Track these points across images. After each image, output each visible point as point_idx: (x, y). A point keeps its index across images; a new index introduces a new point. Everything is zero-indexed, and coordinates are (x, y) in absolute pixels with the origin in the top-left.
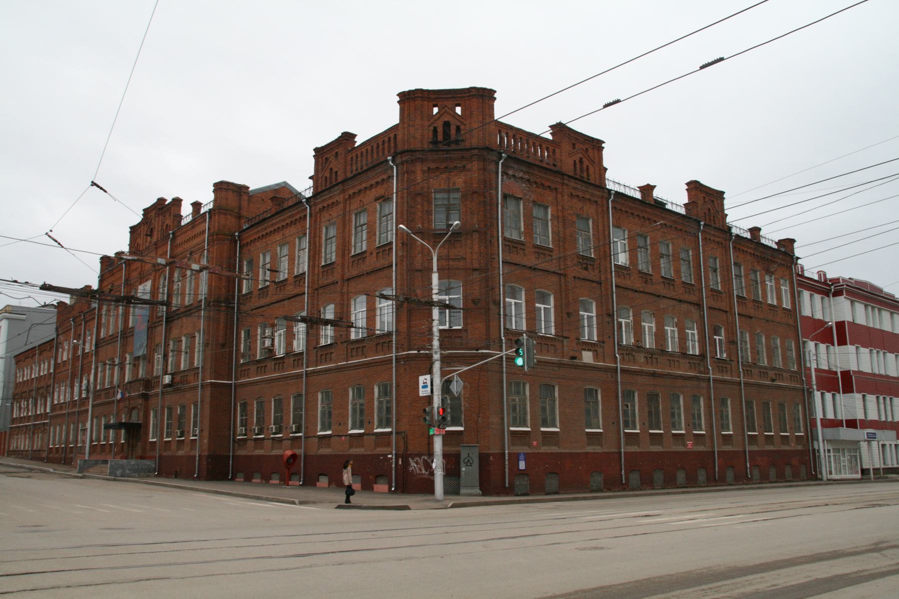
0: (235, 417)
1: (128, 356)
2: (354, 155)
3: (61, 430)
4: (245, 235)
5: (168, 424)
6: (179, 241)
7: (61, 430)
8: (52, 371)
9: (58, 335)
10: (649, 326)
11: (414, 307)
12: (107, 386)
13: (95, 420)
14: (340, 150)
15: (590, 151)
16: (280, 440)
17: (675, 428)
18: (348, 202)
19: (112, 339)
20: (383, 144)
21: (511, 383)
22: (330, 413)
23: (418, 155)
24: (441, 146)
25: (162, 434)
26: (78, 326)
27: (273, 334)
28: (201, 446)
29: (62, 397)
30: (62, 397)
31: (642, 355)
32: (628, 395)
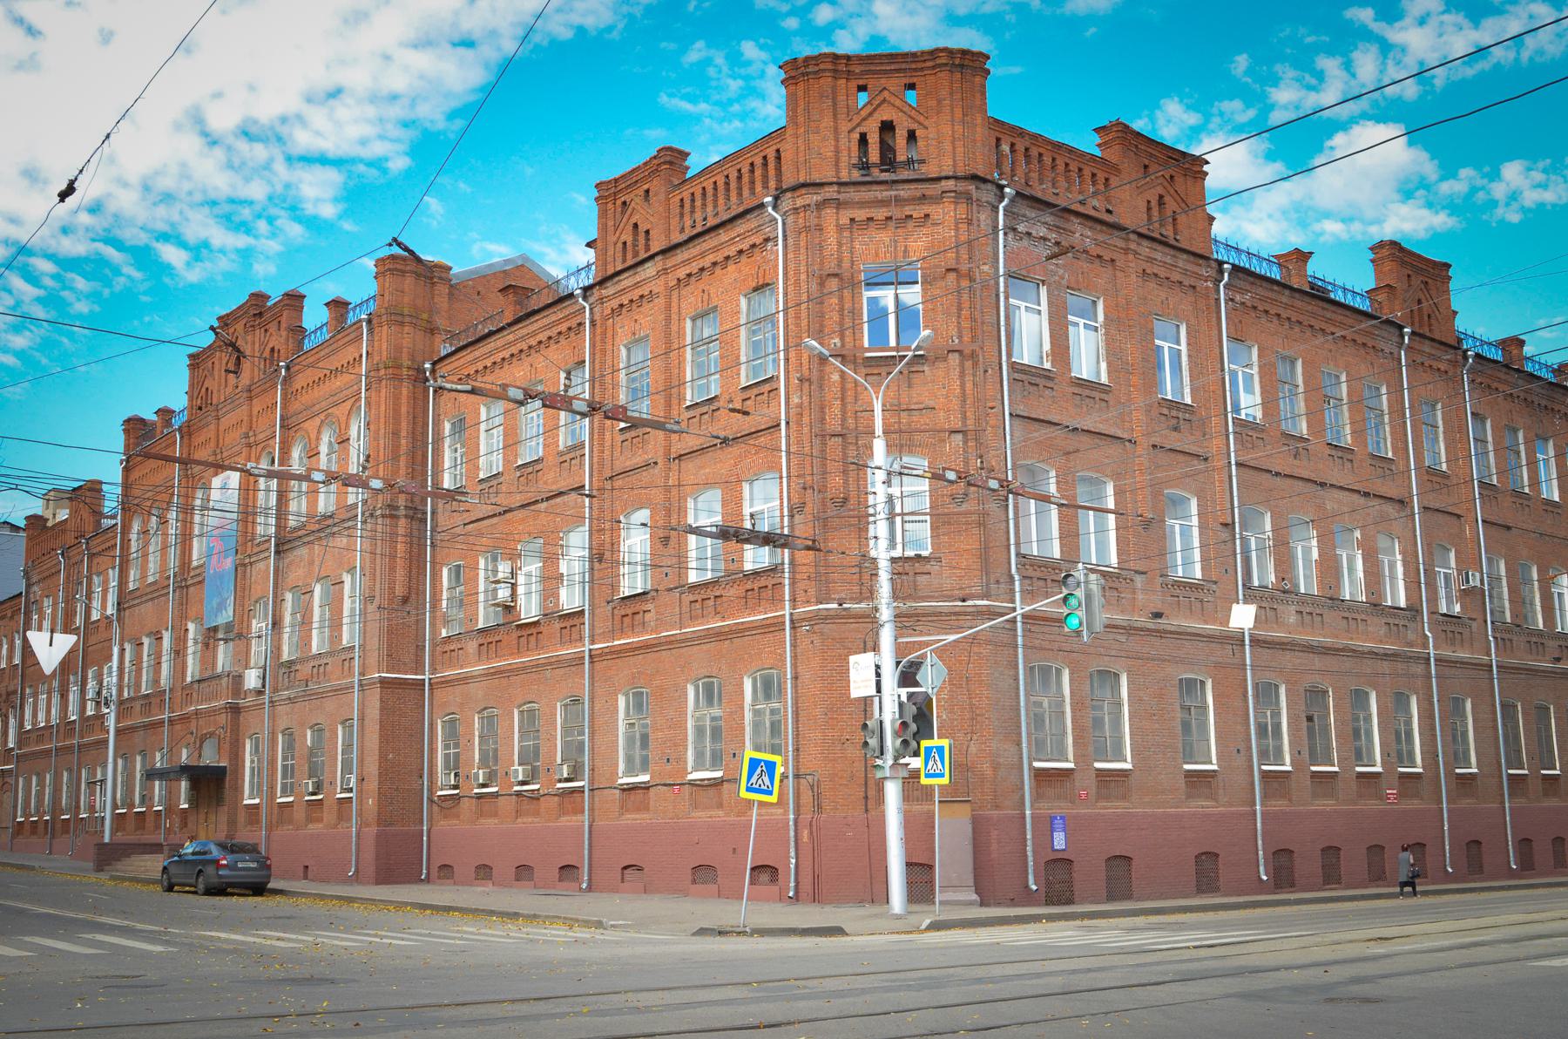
0: (432, 750)
1: (191, 627)
2: (686, 195)
3: (41, 783)
4: (443, 369)
5: (285, 767)
6: (299, 381)
7: (41, 783)
8: (17, 661)
9: (28, 586)
10: (1307, 549)
11: (832, 510)
12: (144, 691)
13: (120, 762)
14: (656, 185)
15: (1179, 180)
16: (535, 797)
17: (1401, 763)
18: (675, 294)
19: (156, 592)
20: (752, 171)
21: (1032, 668)
22: (645, 739)
23: (831, 192)
24: (877, 174)
25: (272, 788)
26: (73, 566)
27: (513, 574)
28: (360, 814)
29: (41, 716)
30: (41, 716)
31: (1293, 608)
32: (1266, 693)
